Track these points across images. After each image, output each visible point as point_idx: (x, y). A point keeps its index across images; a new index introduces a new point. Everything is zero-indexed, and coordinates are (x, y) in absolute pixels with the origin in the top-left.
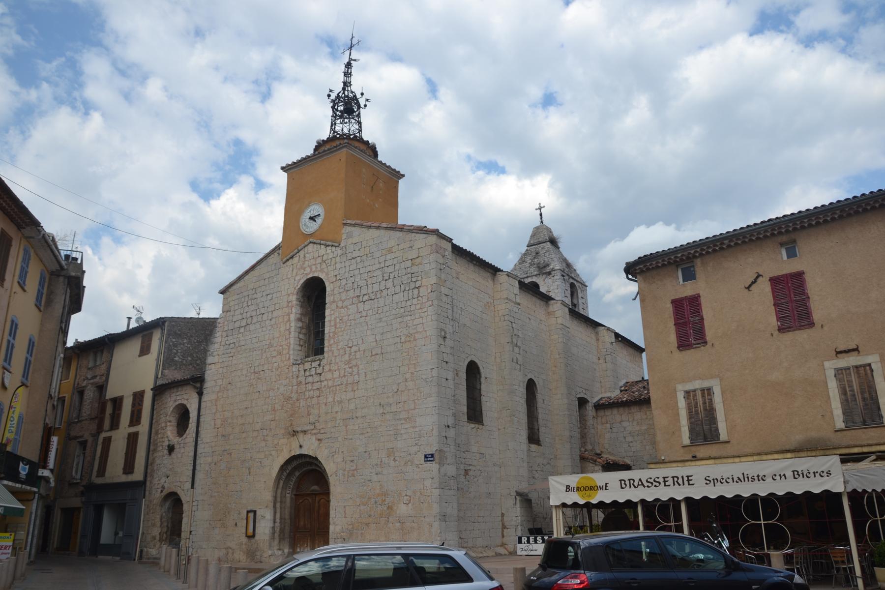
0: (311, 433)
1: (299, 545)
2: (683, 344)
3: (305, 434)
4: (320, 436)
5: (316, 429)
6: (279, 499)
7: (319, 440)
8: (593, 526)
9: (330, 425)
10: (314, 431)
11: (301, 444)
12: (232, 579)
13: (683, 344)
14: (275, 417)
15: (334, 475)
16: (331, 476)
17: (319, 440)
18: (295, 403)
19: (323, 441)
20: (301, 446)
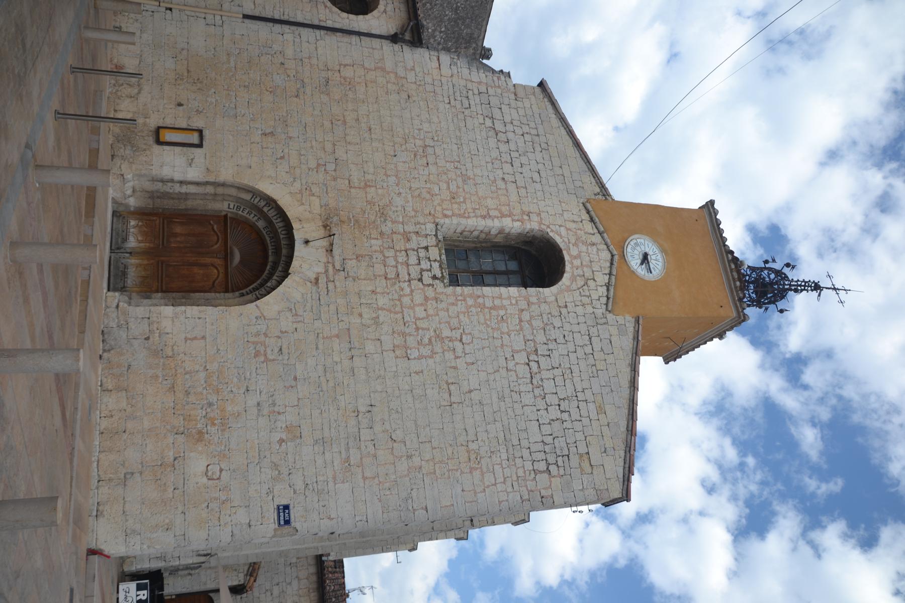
1: (140, 224)
3: (327, 251)
4: (323, 280)
5: (335, 274)
7: (317, 279)
9: (341, 301)
15: (258, 314)
16: (257, 306)
17: (317, 279)
20: (307, 242)
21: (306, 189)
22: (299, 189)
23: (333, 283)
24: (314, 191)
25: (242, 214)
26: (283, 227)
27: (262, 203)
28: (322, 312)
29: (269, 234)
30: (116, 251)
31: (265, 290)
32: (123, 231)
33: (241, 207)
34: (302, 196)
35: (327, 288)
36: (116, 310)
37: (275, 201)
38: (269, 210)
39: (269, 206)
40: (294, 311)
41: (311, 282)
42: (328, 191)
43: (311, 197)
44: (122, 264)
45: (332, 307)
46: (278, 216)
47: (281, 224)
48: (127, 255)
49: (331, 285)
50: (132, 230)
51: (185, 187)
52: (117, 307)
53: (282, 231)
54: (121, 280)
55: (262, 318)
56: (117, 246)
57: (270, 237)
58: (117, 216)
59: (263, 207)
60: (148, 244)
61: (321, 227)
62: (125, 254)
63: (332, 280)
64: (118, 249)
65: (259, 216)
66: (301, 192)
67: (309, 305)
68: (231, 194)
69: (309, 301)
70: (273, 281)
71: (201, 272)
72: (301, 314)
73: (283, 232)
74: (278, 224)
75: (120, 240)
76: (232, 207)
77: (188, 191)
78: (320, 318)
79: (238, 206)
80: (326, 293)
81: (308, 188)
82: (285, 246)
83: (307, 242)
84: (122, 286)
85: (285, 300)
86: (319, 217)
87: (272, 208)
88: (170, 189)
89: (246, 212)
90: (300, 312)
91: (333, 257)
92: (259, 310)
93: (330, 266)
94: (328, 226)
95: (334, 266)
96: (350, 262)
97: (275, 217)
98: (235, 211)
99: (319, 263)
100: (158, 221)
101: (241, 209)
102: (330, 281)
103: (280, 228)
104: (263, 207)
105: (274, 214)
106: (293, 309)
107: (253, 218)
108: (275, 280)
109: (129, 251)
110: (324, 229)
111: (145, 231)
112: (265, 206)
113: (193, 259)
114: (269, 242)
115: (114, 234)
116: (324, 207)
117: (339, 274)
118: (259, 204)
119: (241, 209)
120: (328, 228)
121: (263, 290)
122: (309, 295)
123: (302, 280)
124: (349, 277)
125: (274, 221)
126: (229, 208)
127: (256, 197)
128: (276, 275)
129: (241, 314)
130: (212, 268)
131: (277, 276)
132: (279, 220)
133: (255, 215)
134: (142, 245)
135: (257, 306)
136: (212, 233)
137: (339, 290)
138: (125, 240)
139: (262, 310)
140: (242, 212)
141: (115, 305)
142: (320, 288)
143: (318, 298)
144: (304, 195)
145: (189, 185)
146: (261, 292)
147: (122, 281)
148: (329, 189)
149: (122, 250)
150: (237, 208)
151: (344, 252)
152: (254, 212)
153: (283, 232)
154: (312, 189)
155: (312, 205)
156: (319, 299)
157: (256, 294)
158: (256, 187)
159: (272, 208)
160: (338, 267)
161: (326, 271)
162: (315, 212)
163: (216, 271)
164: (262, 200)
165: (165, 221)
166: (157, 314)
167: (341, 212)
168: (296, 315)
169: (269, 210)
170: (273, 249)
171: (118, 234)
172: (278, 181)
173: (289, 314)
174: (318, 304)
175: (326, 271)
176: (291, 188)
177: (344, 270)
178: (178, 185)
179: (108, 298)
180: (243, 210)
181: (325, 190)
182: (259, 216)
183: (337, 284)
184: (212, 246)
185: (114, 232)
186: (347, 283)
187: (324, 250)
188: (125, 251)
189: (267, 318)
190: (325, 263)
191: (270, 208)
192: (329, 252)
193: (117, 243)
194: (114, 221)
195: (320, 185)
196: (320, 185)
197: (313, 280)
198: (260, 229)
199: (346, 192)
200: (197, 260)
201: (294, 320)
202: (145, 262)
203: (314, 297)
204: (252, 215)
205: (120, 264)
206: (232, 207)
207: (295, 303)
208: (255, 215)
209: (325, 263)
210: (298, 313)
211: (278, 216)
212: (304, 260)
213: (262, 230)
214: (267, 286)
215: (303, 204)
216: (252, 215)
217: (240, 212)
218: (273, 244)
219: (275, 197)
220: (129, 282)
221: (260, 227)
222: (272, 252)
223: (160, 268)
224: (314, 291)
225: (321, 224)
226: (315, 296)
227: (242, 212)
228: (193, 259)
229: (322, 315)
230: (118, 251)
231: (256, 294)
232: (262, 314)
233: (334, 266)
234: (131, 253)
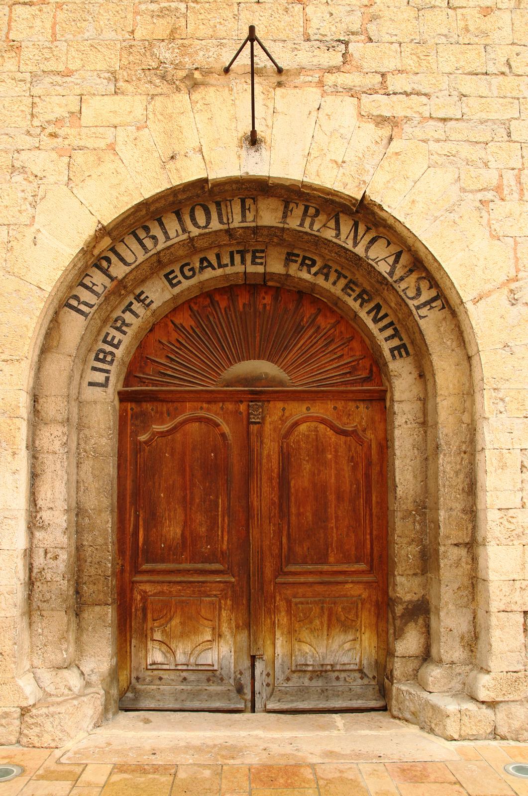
0: (321, 83)
1: (158, 636)
2: (89, 382)
3: (280, 84)
4: (383, 105)
5: (359, 68)
6: (128, 654)
7: (381, 121)
8: (223, 404)
9: (448, 59)
10: (342, 79)
11: (260, 133)
12: (250, 70)
13: (89, 382)
14: (11, 11)
15: (501, 299)
16: (476, 301)
17: (381, 121)
18: (22, 359)
19: (407, 128)
20: (253, 140)
21: (53, 135)
22: (54, 155)
23: (389, 77)
24: (60, 112)
25: (122, 347)
26: (178, 215)
27: (98, 279)
28: (484, 116)
29: (192, 269)
30: (249, 697)
31: (402, 279)
32: (185, 679)
33: (102, 351)
34: (81, 149)
35: (406, 94)
36: (502, 707)
37: (103, 232)
38: (122, 260)
39: (108, 260)
40: (489, 195)
41: (391, 139)
42: (61, 68)
43: (84, 121)
44: (288, 679)
45: (468, 85)
46: (142, 234)
47: (173, 226)
48: (259, 666)
49: (396, 83)
50: (181, 658)
51: (45, 515)
52: (492, 705)
53: (195, 224)
54: (338, 678)
55: (513, 286)
56: (234, 694)
57: (202, 269)
58: (136, 699)
59: (112, 278)
60: (224, 614)
61: (196, 96)
62: (257, 672)
63: (378, 78)
64: (240, 690)
65: (131, 298)
66: (69, 153)
67: (466, 151)
68: (65, 374)
69: (448, 147)
70: (372, 254)
71: (307, 467)
72: (496, 175)
73: (201, 219)
74: (172, 234)
75: (214, 688)
76: (100, 377)
77: (61, 505)
78: (506, 125)
79: (97, 359)
80: (424, 99)
81: (51, 129)
82: (250, 216)
83: (253, 140)
84: (358, 675)
85: (454, 216)
86: (158, 99)
87: (113, 250)
88: (56, 558)
89: (118, 336)
90: (490, 177)
91: (301, 70)
92: (489, 293)
93: (330, 79)
94: (189, 76)
95: (330, 70)
96: (315, 23)
97: (148, 243)
98: (113, 368)
99: (326, 109)
100: (148, 588)
101: (108, 348)
102: (383, 83)
103: (184, 230)
104: (112, 278)
105: (135, 246)
106: (479, 196)
107: (137, 316)
108: (367, 250)
109: (247, 663)
110: (201, 89)
111: (183, 624)
112: (106, 272)
113: (266, 489)
114: (219, 272)
115: (197, 705)
116: (121, 84)
117: (356, 55)
118: (99, 289)
119: (108, 348)
120: (197, 75)
121: (403, 285)
122: (433, 146)
123: (385, 163)
124: (364, 31)
125: (160, 247)
126: (105, 385)
127: (76, 297)
128: (349, 245)
129: (506, 346)
130: (292, 438)
131: (355, 244)
132: (156, 231)
133: (128, 308)
134: (225, 628)
135: (476, 301)
136: (178, 436)
137: (410, 63)
138: (212, 675)
139: (489, 287)
140: (117, 347)
141: (486, 711)
142: (409, 113)
143: (441, 124)
144: (76, 143)
145: (40, 503)
146: (411, 293)
147: (342, 675)
148: (51, 66)
149: (246, 680)
150: (103, 361)
151: (282, 36)
152: (118, 313)
153: (201, 219)
154: (52, 117)
155: (116, 121)
156: (444, 120)
157: (418, 308)
158: (49, 289)
159: (113, 250)
160: (336, 59)
161: (352, 92)
162: (139, 111)
163: (303, 428)
164: (87, 281)
165: (146, 567)
166: (514, 590)
167: (138, 35)
168: (498, 189)
169: (122, 260)
170: (243, 261)
171: (195, 695)
172: (24, 219)
173: (499, 209)
174: (460, 125)
175: (352, 92)
176: (51, 179)
177: (346, 43)
178: (38, 535)
179: (466, 731)
180: (111, 344)
181: (58, 79)
182: (131, 298)
183: (389, 65)
184: (223, 435)
185: (189, 705)
186: (387, 38)
187: (279, 91)
188: (248, 674)
189: (513, 274)
190: (324, 94)
191: (114, 259)
192: (283, 78)
193: (225, 695)
194: (152, 706)
195: (36, 91)
196: (36, 91)
197: (385, 132)
198: (175, 298)
199: (61, 16)
200: (271, 479)
201: (516, 196)
202: (283, 618)
203: (440, 135)
204: (128, 317)
205: (290, 684)
206: (100, 377)
207: (463, 190)
208: (128, 308)
209: (324, 94)
210: (495, 182)
211: (142, 234)
212: (314, 153)
213: (177, 290)
214: (391, 273)
215: (112, 147)
216: (128, 317)
217: (119, 353)
218: (226, 260)
219: (88, 230)
220: (345, 660)
221: (168, 296)
222: (253, 263)
223: (302, 579)
224: (419, 133)
225: (184, 97)
226: (433, 129)
227: (117, 347)
228: (266, 489)
229: (493, 116)
230: (248, 690)
231: (418, 308)
232: (504, 284)
233: (330, 70)
234: (253, 658)
